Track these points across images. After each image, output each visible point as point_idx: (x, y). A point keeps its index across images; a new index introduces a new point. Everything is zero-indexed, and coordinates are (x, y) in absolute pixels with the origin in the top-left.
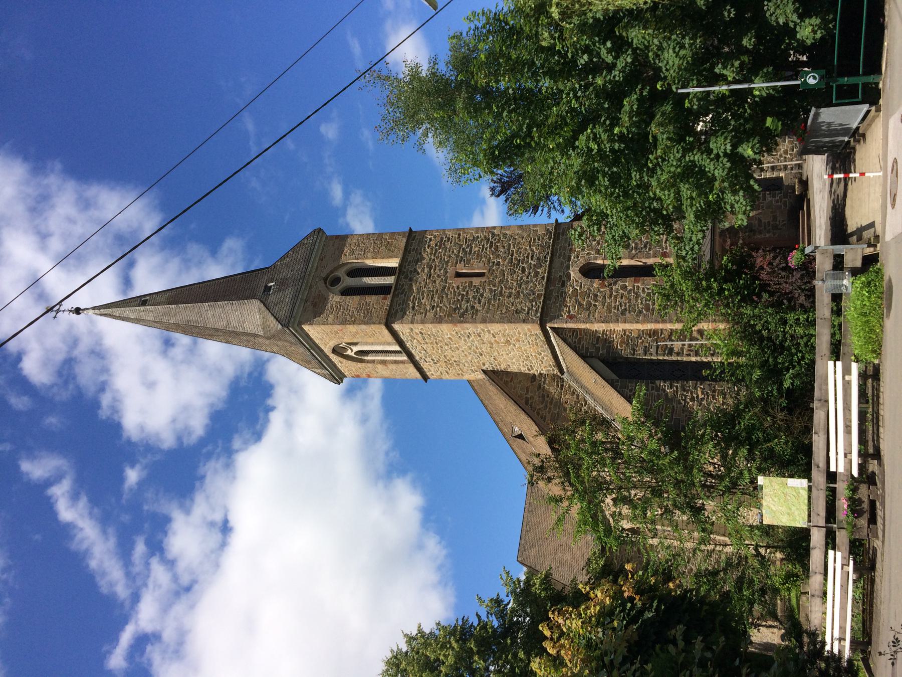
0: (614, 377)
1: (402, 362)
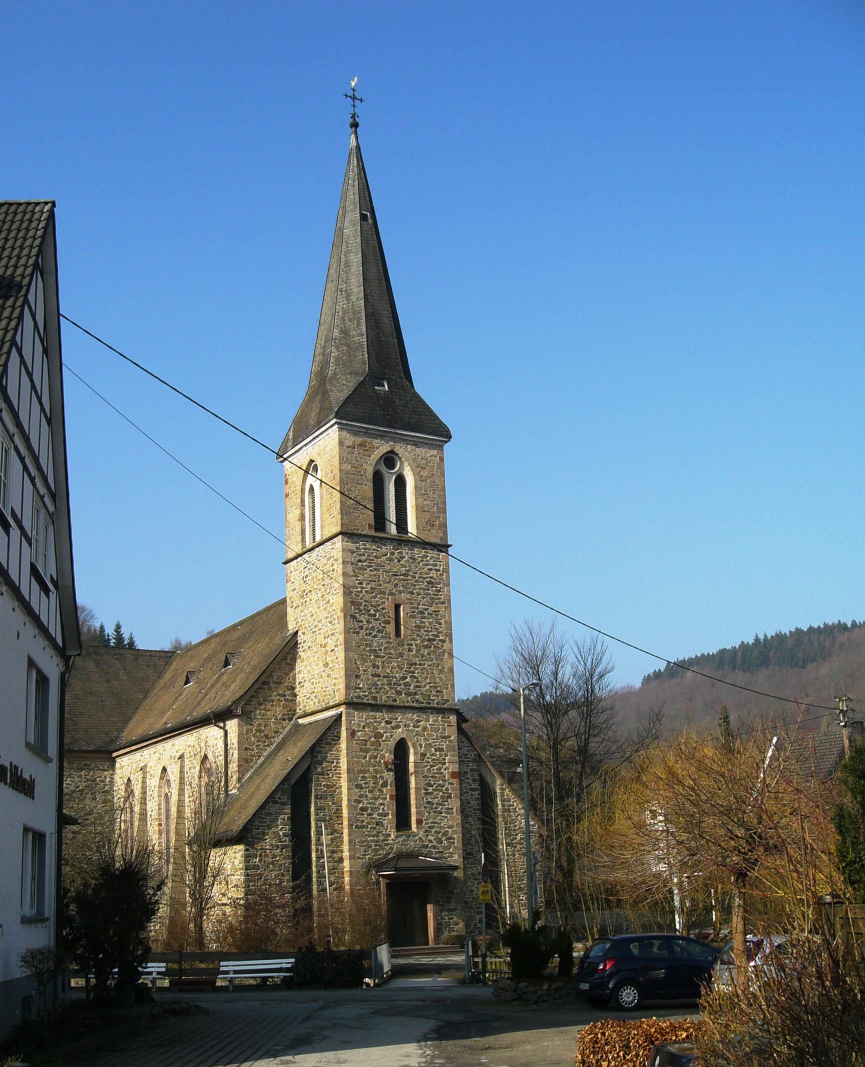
0: (293, 781)
1: (303, 540)
